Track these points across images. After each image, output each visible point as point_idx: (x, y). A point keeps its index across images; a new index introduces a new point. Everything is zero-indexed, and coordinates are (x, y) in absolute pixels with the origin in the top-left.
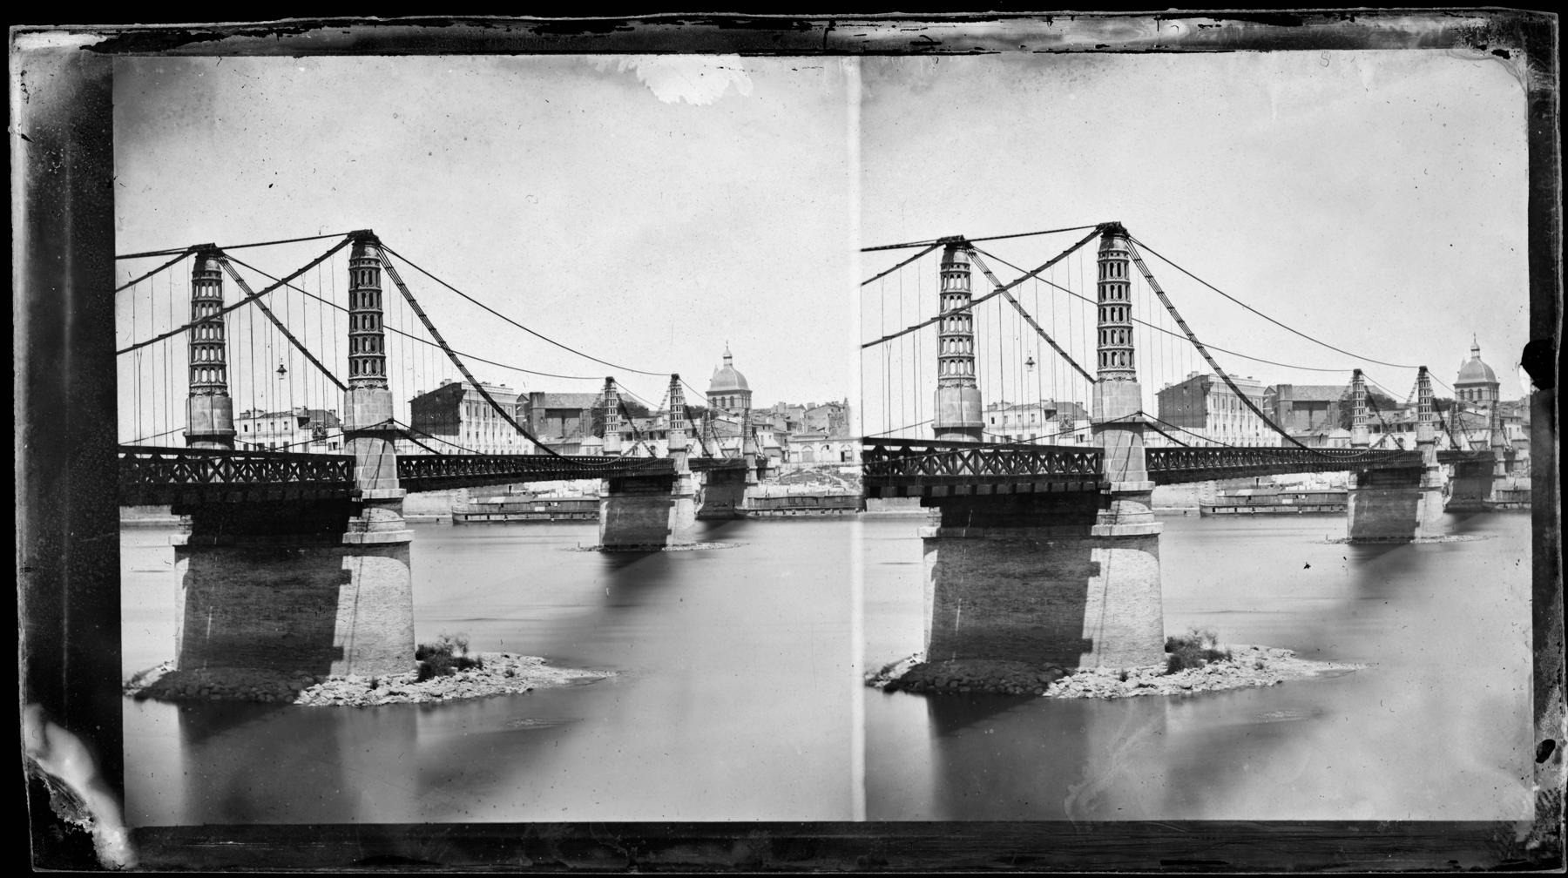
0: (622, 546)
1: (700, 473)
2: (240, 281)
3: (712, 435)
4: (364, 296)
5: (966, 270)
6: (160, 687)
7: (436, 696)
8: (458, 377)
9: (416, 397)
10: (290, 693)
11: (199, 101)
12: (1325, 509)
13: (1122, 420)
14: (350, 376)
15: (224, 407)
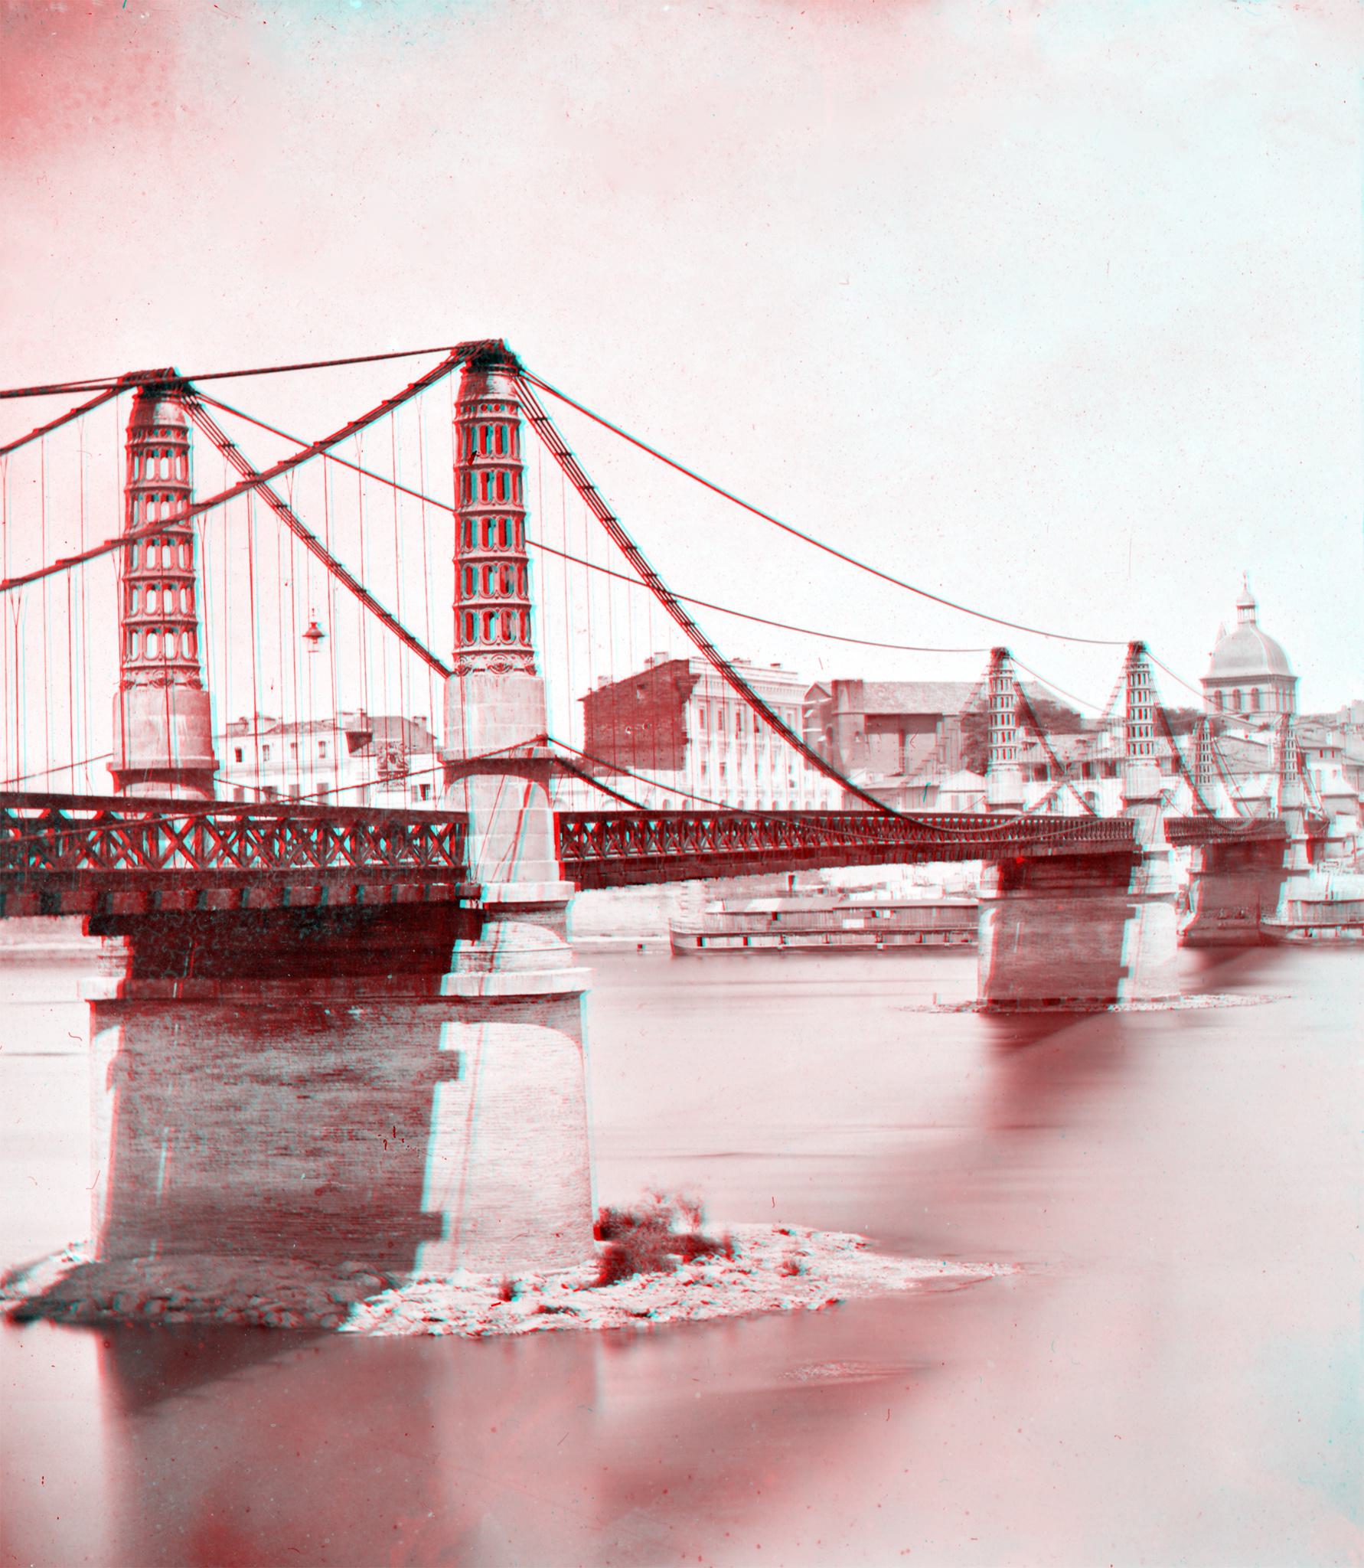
0: (1026, 1002)
1: (1188, 849)
2: (226, 446)
3: (1213, 770)
4: (486, 478)
5: (180, 441)
6: (61, 1297)
7: (638, 1315)
8: (682, 648)
9: (595, 689)
10: (332, 1308)
11: (141, 70)
12: (931, 940)
13: (505, 755)
14: (456, 647)
15: (193, 711)
